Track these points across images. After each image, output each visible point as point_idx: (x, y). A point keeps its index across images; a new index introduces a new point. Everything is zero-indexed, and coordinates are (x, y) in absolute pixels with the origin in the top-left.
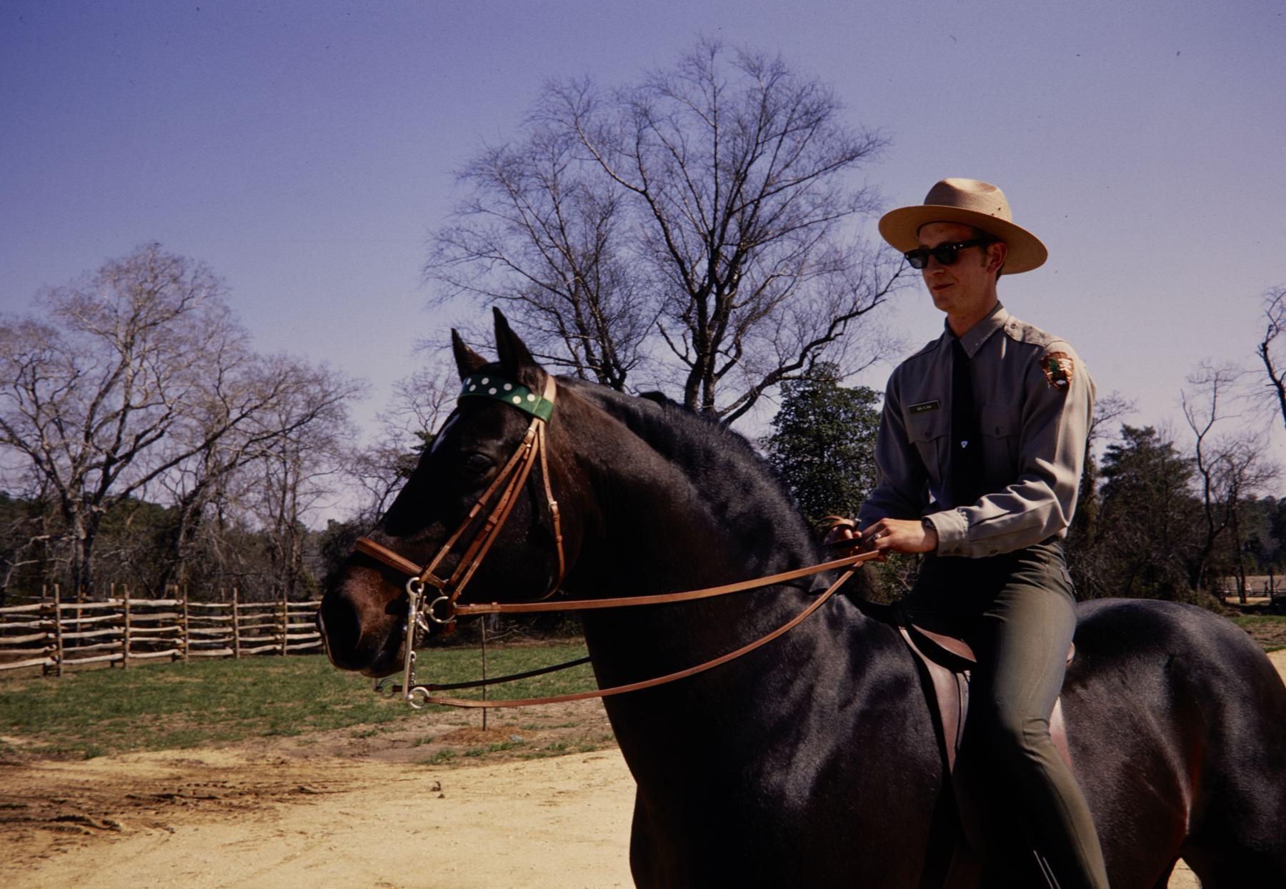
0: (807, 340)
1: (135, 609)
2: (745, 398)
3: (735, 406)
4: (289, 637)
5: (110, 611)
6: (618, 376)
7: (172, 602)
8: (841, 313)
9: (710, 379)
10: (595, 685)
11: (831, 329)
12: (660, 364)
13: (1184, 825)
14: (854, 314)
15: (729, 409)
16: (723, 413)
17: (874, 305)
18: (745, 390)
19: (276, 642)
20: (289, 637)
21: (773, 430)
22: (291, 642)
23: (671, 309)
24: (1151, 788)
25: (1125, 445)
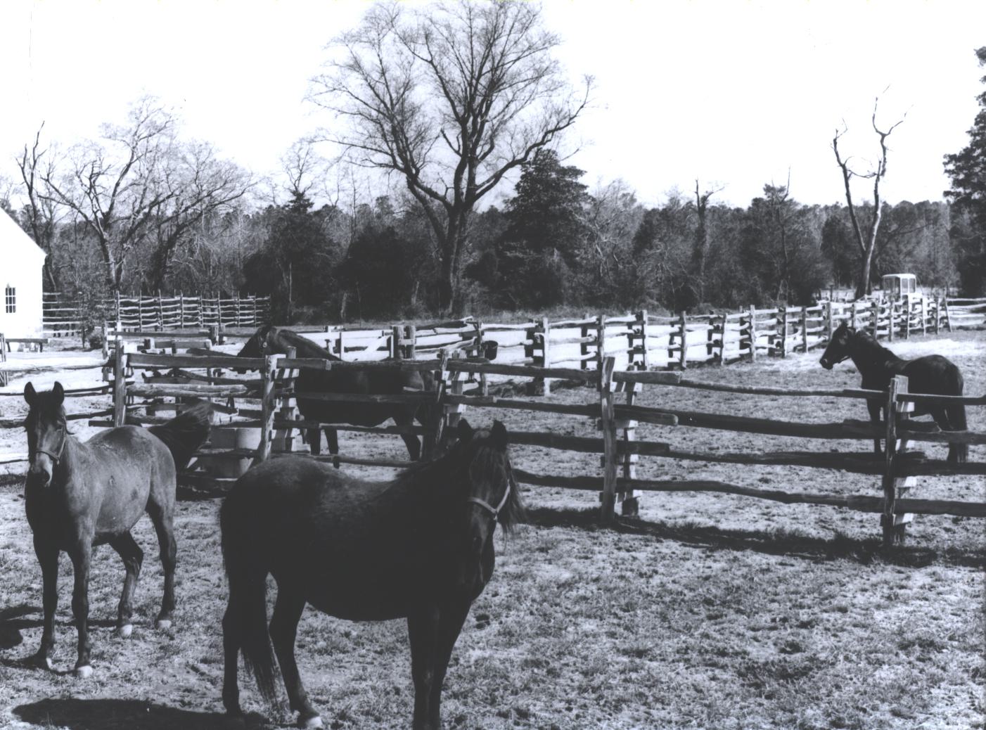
0: (529, 145)
1: (222, 304)
2: (492, 178)
3: (488, 181)
4: (164, 313)
5: (175, 302)
6: (414, 171)
7: (195, 299)
8: (549, 128)
9: (473, 167)
10: (860, 383)
11: (544, 137)
12: (440, 164)
13: (438, 428)
14: (557, 129)
15: (484, 184)
16: (481, 186)
17: (568, 124)
18: (491, 174)
19: (234, 320)
20: (164, 313)
21: (515, 194)
22: (242, 320)
23: (978, 138)
24: (378, 398)
25: (765, 197)
